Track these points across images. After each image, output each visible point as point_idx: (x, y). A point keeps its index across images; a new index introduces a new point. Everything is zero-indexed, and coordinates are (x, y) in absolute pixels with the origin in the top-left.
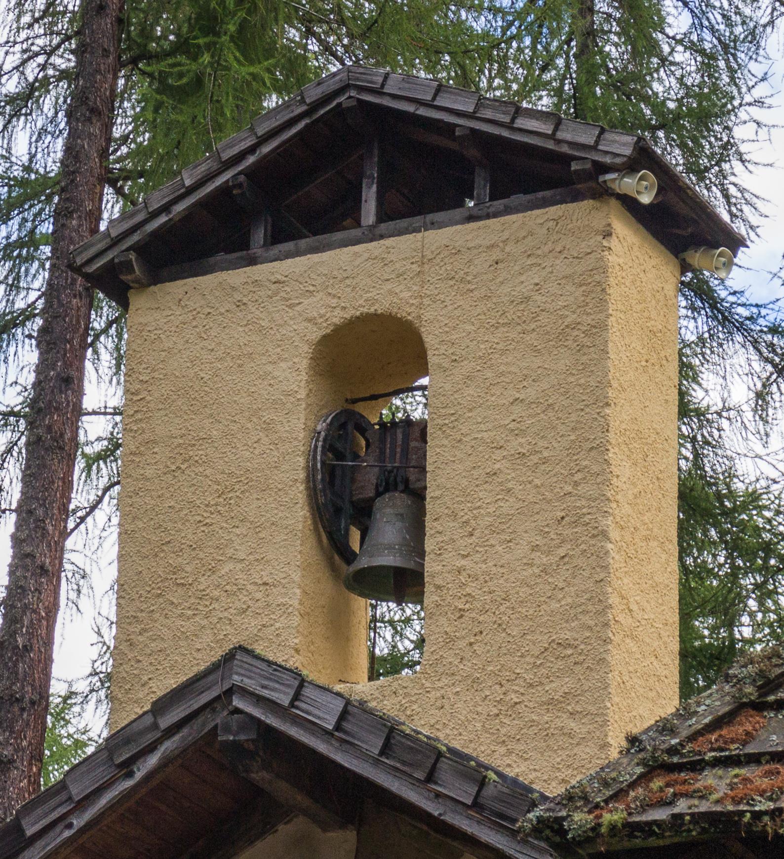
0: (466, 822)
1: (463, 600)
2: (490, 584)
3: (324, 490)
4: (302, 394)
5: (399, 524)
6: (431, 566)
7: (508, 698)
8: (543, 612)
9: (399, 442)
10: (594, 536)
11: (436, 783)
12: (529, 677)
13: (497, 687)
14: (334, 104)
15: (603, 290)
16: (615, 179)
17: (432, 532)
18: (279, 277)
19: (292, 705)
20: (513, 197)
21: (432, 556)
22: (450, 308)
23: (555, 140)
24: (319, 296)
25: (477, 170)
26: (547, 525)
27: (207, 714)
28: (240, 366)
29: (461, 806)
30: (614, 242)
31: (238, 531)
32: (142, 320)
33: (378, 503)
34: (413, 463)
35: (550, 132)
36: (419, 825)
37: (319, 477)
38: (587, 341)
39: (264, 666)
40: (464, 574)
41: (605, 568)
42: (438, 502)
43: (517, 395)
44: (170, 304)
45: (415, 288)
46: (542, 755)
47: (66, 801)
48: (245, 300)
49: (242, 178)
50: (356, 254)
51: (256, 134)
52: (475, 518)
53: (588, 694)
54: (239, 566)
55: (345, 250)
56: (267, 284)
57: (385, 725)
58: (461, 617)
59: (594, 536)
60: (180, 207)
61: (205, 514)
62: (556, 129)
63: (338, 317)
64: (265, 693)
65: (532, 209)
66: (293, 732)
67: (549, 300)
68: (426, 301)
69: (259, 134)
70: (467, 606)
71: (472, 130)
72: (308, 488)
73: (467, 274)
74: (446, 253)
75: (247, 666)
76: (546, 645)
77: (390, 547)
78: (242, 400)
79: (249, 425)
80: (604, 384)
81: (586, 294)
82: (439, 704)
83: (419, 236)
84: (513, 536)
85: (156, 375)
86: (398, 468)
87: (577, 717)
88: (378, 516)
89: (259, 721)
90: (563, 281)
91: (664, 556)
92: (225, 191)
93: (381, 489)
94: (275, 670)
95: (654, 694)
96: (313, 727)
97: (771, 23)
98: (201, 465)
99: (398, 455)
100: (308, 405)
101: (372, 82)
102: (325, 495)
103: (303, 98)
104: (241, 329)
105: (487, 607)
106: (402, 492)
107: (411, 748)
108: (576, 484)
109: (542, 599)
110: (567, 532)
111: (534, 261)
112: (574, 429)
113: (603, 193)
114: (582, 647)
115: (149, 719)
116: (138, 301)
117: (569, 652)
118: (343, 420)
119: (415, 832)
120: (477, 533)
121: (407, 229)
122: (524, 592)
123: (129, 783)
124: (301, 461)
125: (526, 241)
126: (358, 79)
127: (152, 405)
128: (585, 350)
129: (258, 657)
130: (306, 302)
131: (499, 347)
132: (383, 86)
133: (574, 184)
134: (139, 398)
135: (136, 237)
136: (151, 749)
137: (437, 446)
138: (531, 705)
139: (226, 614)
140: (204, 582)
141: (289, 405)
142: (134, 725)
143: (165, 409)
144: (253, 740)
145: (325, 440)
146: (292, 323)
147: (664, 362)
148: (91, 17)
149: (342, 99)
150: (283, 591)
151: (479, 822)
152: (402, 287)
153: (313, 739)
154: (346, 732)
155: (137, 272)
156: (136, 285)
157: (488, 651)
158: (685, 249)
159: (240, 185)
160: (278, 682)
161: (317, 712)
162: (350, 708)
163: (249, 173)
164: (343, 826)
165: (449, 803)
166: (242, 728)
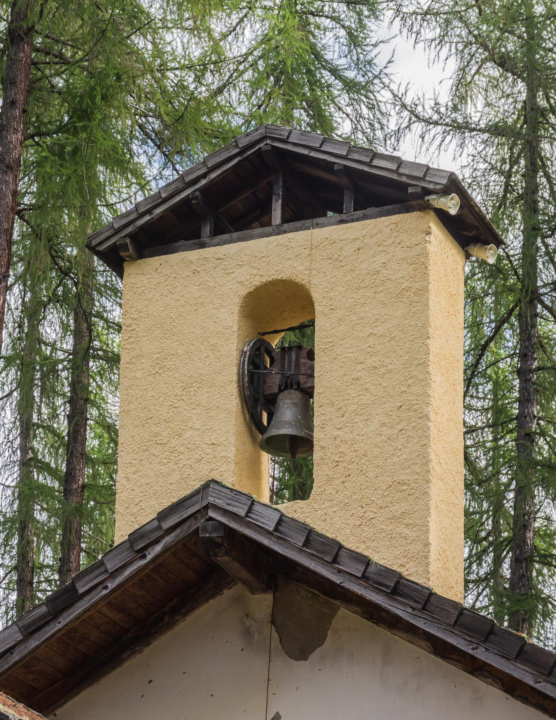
0: (357, 587)
1: (338, 455)
2: (354, 446)
3: (249, 387)
4: (235, 328)
5: (294, 409)
6: (317, 435)
7: (367, 515)
8: (388, 464)
9: (294, 359)
10: (420, 418)
11: (339, 564)
12: (380, 502)
13: (360, 508)
14: (257, 148)
15: (426, 267)
16: (435, 199)
17: (318, 414)
18: (221, 256)
19: (247, 515)
20: (368, 209)
21: (318, 428)
22: (329, 277)
23: (398, 173)
24: (246, 268)
25: (345, 191)
26: (391, 411)
27: (192, 520)
28: (196, 310)
29: (354, 578)
30: (432, 238)
31: (195, 412)
32: (133, 281)
33: (281, 396)
34: (303, 372)
35: (395, 169)
36: (312, 590)
37: (246, 379)
38: (416, 299)
39: (228, 492)
40: (339, 439)
41: (428, 437)
42: (322, 396)
43: (372, 331)
44: (151, 271)
45: (307, 264)
46: (388, 550)
47: (104, 572)
48: (198, 270)
49: (198, 193)
50: (269, 242)
51: (207, 166)
52: (346, 406)
53: (417, 513)
54: (196, 433)
55: (261, 239)
56: (213, 259)
57: (306, 529)
58: (337, 465)
59: (420, 418)
60: (158, 211)
61: (174, 401)
62: (399, 167)
63: (257, 281)
64: (230, 508)
65: (381, 216)
66: (248, 532)
67: (392, 273)
68: (314, 272)
69: (209, 166)
70: (341, 459)
71: (345, 166)
72: (239, 386)
73: (339, 256)
74: (327, 243)
75: (217, 492)
76: (391, 484)
77: (289, 423)
78: (197, 331)
79: (202, 347)
80: (426, 325)
81: (415, 270)
82: (323, 518)
83: (309, 232)
84: (369, 417)
85: (142, 315)
86: (293, 375)
87: (410, 527)
88: (281, 404)
89: (225, 526)
90: (401, 262)
91: (457, 432)
92: (186, 201)
93: (282, 388)
94: (236, 494)
95: (451, 514)
96: (259, 529)
97: (408, 127)
98: (171, 371)
99: (293, 368)
100: (239, 335)
101: (281, 135)
102: (250, 391)
103: (237, 144)
104: (196, 288)
105: (353, 460)
106: (295, 390)
107: (323, 542)
108: (409, 386)
109: (388, 456)
110: (404, 415)
111: (383, 249)
112: (407, 352)
113: (425, 207)
114: (413, 485)
115: (156, 523)
116: (130, 269)
117: (405, 487)
118: (258, 345)
119: (309, 595)
120: (347, 415)
121: (301, 227)
122: (377, 451)
123: (143, 562)
124: (235, 370)
125: (377, 236)
126: (272, 133)
127: (139, 334)
128: (414, 304)
129: (224, 487)
130: (237, 271)
131: (360, 301)
132: (288, 137)
133: (409, 201)
134: (131, 329)
135: (130, 229)
136: (157, 541)
137: (321, 361)
138: (381, 519)
139: (188, 462)
140: (174, 442)
141: (227, 335)
142: (146, 526)
143: (148, 336)
144: (220, 537)
145: (249, 357)
146: (228, 284)
147: (457, 314)
148: (7, 108)
149: (261, 145)
150: (224, 448)
151: (365, 588)
152: (298, 263)
153: (259, 536)
154: (281, 533)
155: (131, 251)
156: (129, 259)
157: (354, 487)
158: (468, 245)
159: (196, 198)
160: (237, 501)
161: (262, 520)
162: (283, 518)
163: (202, 190)
164: (265, 591)
165: (346, 575)
166: (215, 529)
